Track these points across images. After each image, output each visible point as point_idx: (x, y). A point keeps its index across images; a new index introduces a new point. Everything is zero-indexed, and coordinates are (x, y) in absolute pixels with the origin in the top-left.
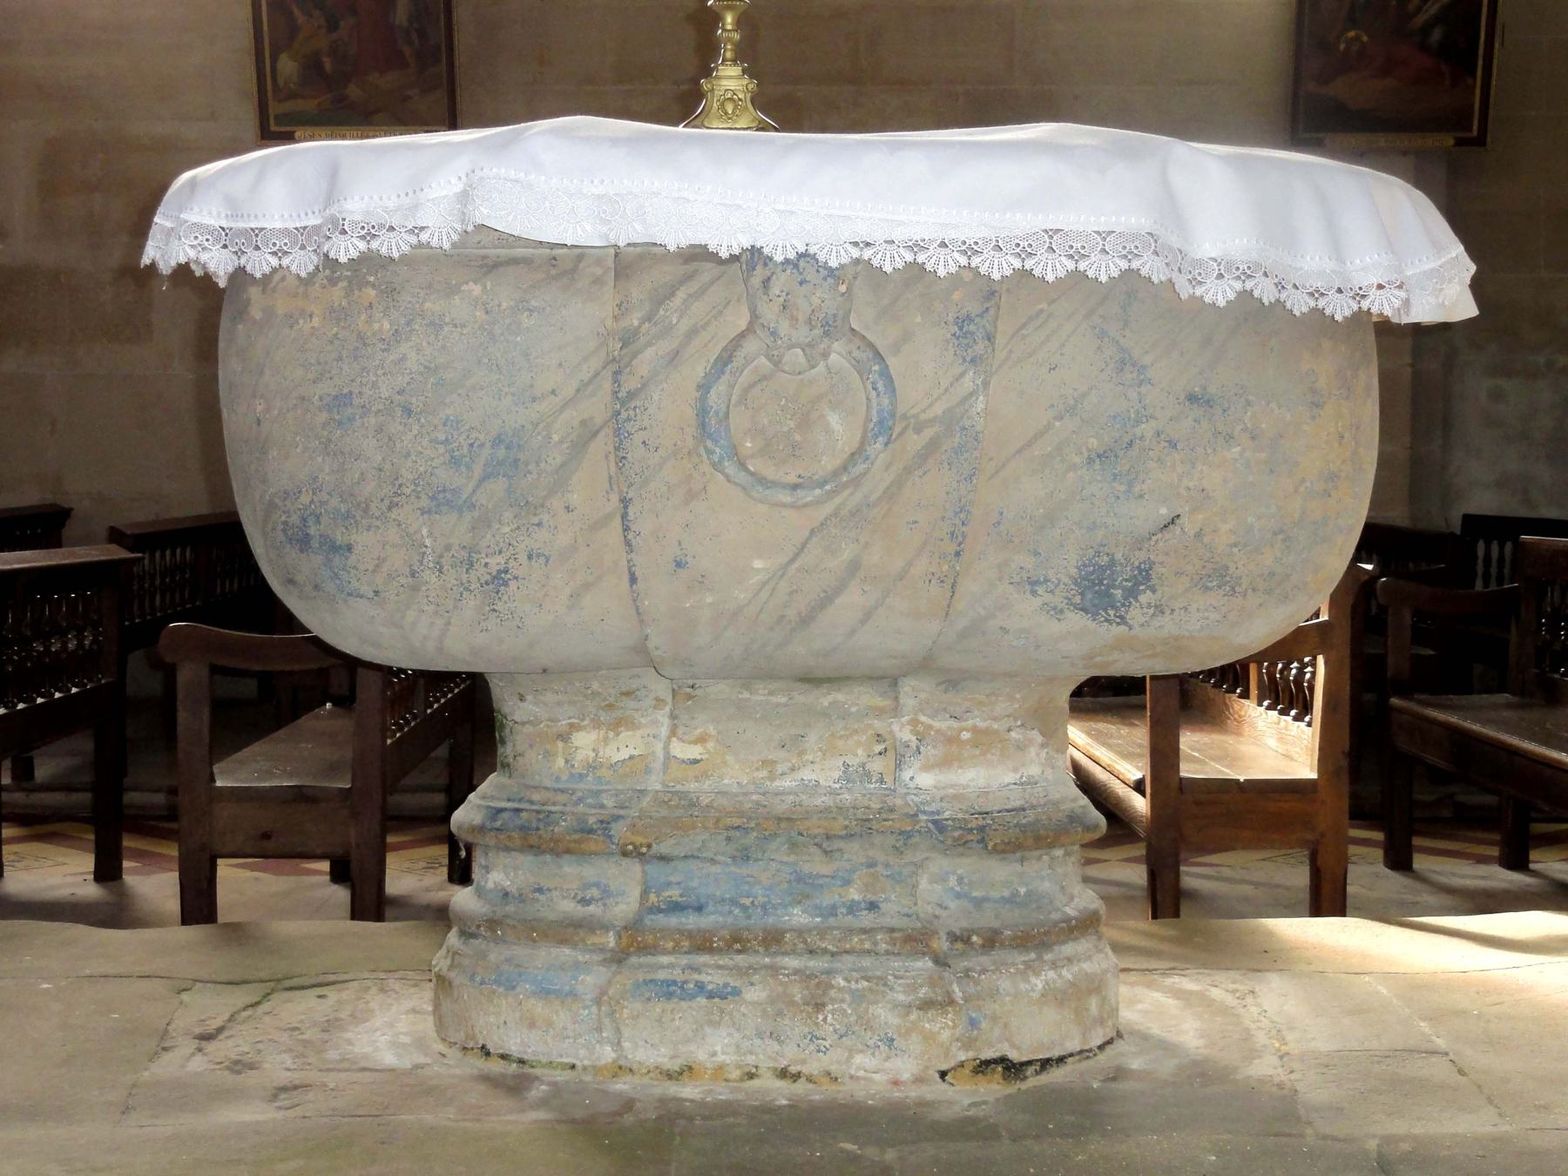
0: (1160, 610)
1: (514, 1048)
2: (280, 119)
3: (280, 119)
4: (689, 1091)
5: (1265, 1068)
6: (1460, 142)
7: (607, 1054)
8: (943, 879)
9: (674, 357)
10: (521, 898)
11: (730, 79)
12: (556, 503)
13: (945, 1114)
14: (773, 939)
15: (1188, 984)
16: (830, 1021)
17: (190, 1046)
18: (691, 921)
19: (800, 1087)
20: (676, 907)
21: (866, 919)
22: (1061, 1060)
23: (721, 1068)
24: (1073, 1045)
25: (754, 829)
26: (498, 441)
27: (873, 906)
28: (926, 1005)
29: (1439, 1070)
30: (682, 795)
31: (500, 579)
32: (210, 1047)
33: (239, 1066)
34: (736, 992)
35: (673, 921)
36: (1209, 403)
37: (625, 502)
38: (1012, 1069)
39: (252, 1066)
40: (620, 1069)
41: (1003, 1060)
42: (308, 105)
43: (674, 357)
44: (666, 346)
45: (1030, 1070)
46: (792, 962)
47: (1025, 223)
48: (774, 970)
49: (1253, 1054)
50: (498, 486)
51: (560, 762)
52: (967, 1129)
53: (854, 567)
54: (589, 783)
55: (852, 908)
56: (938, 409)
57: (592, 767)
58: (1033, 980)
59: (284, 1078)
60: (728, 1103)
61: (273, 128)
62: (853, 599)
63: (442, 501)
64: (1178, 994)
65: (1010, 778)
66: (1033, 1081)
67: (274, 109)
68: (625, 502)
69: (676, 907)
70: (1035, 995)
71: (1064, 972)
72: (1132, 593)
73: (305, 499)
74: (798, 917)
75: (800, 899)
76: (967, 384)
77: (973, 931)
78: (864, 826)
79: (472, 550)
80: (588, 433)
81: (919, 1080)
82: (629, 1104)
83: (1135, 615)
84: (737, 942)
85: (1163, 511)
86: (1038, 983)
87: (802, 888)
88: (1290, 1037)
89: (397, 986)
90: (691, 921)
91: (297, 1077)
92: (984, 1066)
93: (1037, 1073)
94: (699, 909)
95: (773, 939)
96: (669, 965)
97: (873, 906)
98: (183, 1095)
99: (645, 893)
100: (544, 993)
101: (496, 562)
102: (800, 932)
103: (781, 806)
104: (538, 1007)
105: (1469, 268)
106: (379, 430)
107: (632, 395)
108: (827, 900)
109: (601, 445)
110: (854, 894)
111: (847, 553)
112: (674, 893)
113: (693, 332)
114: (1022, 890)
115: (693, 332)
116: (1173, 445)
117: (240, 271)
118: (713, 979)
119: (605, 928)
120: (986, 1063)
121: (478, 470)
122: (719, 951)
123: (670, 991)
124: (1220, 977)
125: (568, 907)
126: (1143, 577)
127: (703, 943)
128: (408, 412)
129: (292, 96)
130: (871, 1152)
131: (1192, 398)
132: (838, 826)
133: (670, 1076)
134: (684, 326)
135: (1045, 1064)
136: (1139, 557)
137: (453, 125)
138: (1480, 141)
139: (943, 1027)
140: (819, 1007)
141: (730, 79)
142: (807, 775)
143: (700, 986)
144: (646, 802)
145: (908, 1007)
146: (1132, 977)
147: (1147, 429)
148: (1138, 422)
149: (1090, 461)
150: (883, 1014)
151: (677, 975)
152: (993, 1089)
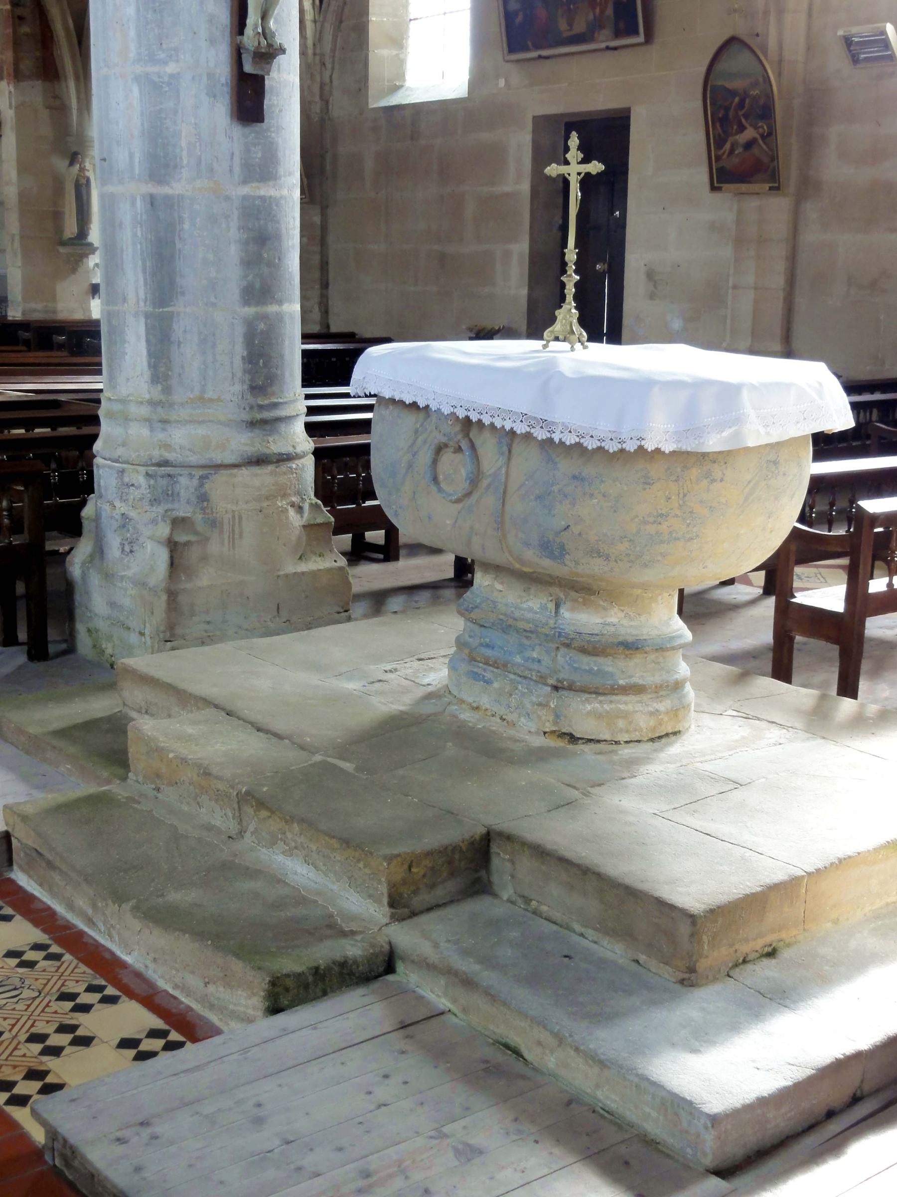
16: (513, 702)
18: (489, 652)
21: (535, 666)
22: (599, 741)
24: (607, 737)
28: (540, 704)
36: (582, 480)
45: (580, 741)
55: (533, 660)
58: (587, 705)
65: (599, 621)
70: (584, 712)
71: (605, 706)
74: (518, 659)
75: (520, 652)
77: (565, 680)
84: (495, 665)
85: (563, 523)
86: (589, 707)
87: (521, 649)
92: (562, 735)
93: (583, 743)
97: (539, 661)
103: (517, 614)
110: (535, 655)
114: (596, 668)
116: (565, 496)
118: (488, 675)
120: (565, 734)
122: (490, 665)
131: (575, 477)
137: (788, 353)
148: (552, 485)
149: (536, 499)
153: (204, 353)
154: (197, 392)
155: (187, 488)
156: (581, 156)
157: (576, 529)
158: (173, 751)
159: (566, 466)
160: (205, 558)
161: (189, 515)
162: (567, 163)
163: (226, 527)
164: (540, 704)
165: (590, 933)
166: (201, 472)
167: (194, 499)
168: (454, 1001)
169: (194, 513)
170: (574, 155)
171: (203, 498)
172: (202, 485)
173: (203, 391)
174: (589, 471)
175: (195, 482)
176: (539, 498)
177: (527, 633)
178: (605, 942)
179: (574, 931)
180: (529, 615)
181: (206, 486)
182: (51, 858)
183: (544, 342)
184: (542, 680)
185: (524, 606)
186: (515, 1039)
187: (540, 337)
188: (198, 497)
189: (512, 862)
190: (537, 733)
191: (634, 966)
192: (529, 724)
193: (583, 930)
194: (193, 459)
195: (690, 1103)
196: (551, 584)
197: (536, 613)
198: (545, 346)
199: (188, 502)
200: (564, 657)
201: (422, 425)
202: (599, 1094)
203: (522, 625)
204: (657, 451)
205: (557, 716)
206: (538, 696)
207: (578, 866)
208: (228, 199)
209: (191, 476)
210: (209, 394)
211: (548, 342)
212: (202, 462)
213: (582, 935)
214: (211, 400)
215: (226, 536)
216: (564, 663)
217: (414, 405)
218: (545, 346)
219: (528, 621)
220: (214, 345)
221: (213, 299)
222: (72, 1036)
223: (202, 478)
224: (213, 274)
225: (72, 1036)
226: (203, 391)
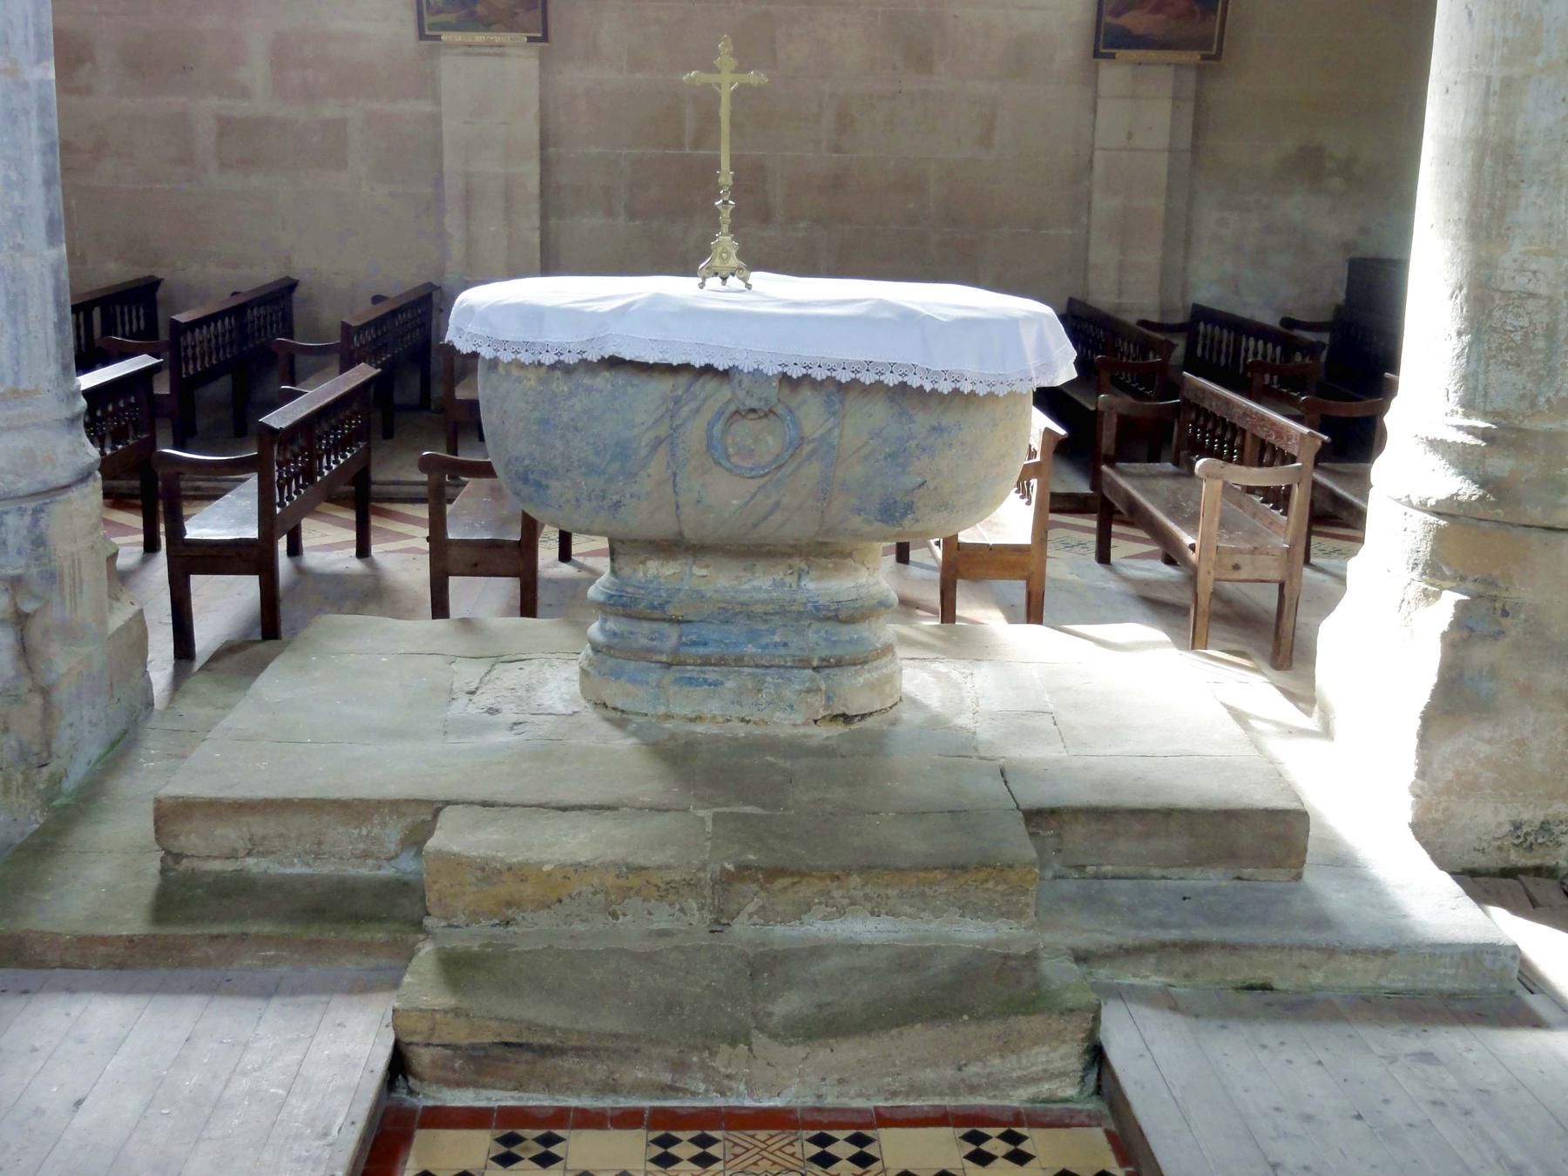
0: (917, 521)
1: (619, 705)
2: (433, 26)
3: (433, 26)
4: (700, 728)
5: (964, 720)
6: (1204, 58)
7: (662, 710)
8: (818, 632)
9: (698, 410)
10: (622, 636)
11: (725, 242)
12: (643, 473)
13: (814, 742)
14: (739, 661)
15: (941, 667)
16: (764, 697)
17: (464, 699)
18: (702, 650)
19: (750, 727)
20: (694, 644)
21: (782, 651)
23: (714, 717)
24: (877, 707)
25: (731, 612)
26: (617, 444)
27: (785, 645)
28: (809, 691)
29: (1046, 723)
30: (698, 592)
31: (617, 505)
32: (475, 698)
33: (492, 711)
34: (722, 683)
35: (693, 650)
37: (675, 474)
38: (847, 719)
39: (497, 711)
40: (668, 717)
41: (844, 715)
42: (450, 18)
43: (698, 410)
44: (694, 405)
46: (747, 670)
47: (859, 356)
48: (740, 673)
49: (961, 713)
50: (616, 466)
51: (641, 574)
52: (824, 751)
53: (777, 504)
54: (655, 585)
55: (776, 645)
56: (817, 435)
57: (656, 577)
59: (515, 718)
60: (716, 735)
61: (428, 32)
62: (778, 517)
63: (591, 470)
64: (936, 674)
66: (856, 726)
67: (428, 20)
68: (675, 474)
69: (694, 644)
72: (904, 515)
73: (527, 462)
74: (750, 649)
76: (830, 424)
78: (782, 612)
79: (604, 491)
80: (658, 442)
81: (805, 724)
82: (673, 736)
83: (906, 523)
84: (721, 662)
87: (753, 636)
88: (981, 702)
89: (556, 663)
90: (702, 650)
91: (520, 718)
94: (705, 644)
95: (739, 661)
96: (692, 671)
97: (785, 645)
98: (467, 728)
99: (680, 637)
100: (633, 681)
101: (616, 498)
102: (752, 656)
103: (744, 598)
104: (629, 687)
105: (1073, 354)
106: (562, 437)
107: (678, 427)
108: (764, 641)
109: (664, 448)
110: (777, 639)
111: (774, 498)
112: (694, 637)
113: (706, 399)
115: (706, 399)
117: (496, 358)
119: (662, 652)
121: (608, 458)
123: (690, 681)
124: (959, 664)
125: (644, 641)
126: (910, 507)
127: (706, 662)
128: (576, 429)
129: (439, 12)
130: (781, 762)
132: (770, 608)
133: (691, 720)
134: (702, 396)
135: (863, 716)
136: (907, 499)
138: (1217, 57)
139: (817, 701)
140: (760, 691)
141: (725, 242)
142: (756, 583)
143: (705, 680)
144: (681, 595)
145: (800, 692)
146: (916, 663)
147: (913, 443)
150: (787, 693)
151: (695, 675)
152: (839, 729)
153: (14, 322)
154: (9, 382)
155: (16, 531)
156: (733, 63)
157: (931, 485)
158: (547, 862)
159: (922, 420)
160: (46, 633)
161: (19, 571)
162: (714, 70)
163: (67, 580)
164: (809, 691)
165: (1175, 871)
166: (30, 505)
167: (27, 546)
168: (1170, 973)
169: (28, 566)
170: (725, 61)
171: (39, 542)
172: (35, 523)
173: (17, 382)
174: (948, 419)
175: (28, 519)
176: (892, 456)
177: (766, 617)
178: (1197, 873)
179: (1152, 878)
180: (764, 596)
181: (42, 523)
182: (1537, 862)
183: (699, 280)
184: (803, 663)
185: (747, 587)
186: (1258, 975)
187: (693, 274)
188: (33, 543)
189: (1059, 836)
190: (805, 724)
191: (1238, 883)
192: (793, 716)
193: (1164, 872)
194: (24, 485)
195: (1493, 945)
196: (790, 556)
197: (769, 592)
198: (702, 286)
199: (19, 552)
200: (818, 632)
201: (687, 391)
202: (1383, 982)
203: (758, 609)
204: (973, 393)
205: (829, 699)
206: (803, 682)
207: (1156, 811)
208: (25, 86)
209: (22, 512)
210: (25, 385)
211: (704, 279)
212: (36, 487)
213: (1164, 877)
214: (27, 393)
215: (67, 589)
216: (814, 639)
217: (708, 369)
218: (702, 286)
219: (763, 602)
220: (25, 311)
221: (19, 240)
222: (1011, 1148)
223: (36, 511)
224: (17, 201)
225: (1011, 1148)
226: (17, 382)
